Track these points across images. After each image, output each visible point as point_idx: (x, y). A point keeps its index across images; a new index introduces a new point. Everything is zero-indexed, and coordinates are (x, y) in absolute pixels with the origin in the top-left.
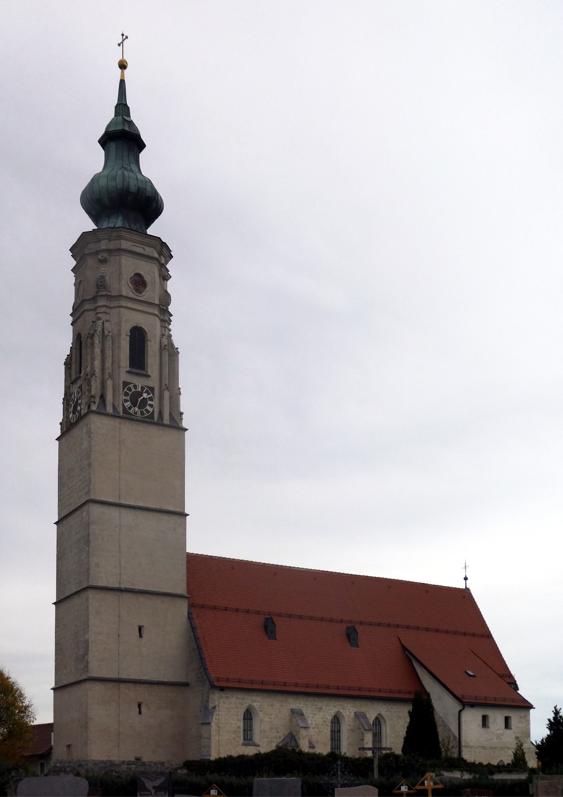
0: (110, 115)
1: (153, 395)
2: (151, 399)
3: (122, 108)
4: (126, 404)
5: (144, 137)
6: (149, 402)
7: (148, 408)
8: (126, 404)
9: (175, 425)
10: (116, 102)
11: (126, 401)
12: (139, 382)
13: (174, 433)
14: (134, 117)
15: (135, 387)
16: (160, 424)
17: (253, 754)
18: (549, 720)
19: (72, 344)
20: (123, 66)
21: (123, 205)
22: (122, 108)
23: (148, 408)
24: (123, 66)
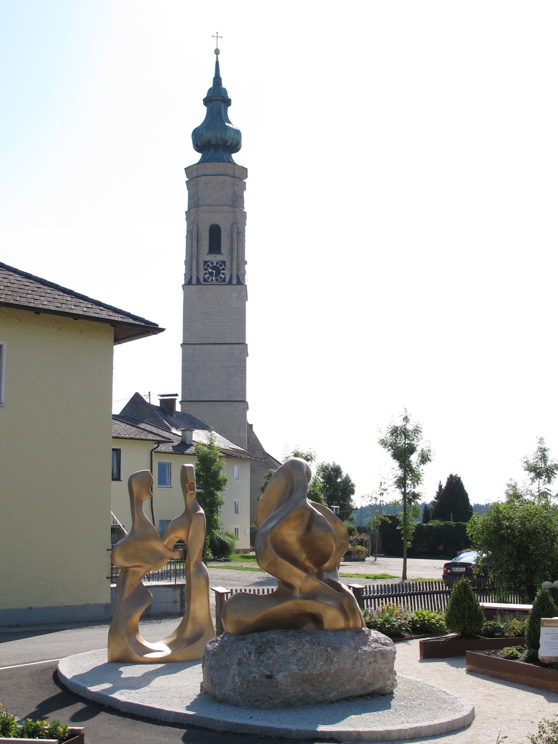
0: (210, 84)
1: (225, 266)
2: (223, 269)
3: (217, 80)
4: (205, 276)
5: (230, 96)
6: (222, 272)
7: (221, 275)
8: (205, 276)
9: (238, 280)
10: (213, 76)
11: (206, 274)
12: (215, 258)
13: (239, 287)
14: (224, 85)
15: (212, 263)
16: (230, 283)
17: (202, 676)
18: (440, 486)
19: (245, 213)
20: (217, 52)
21: (216, 141)
22: (217, 80)
23: (221, 275)
24: (217, 52)
